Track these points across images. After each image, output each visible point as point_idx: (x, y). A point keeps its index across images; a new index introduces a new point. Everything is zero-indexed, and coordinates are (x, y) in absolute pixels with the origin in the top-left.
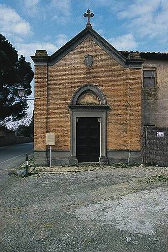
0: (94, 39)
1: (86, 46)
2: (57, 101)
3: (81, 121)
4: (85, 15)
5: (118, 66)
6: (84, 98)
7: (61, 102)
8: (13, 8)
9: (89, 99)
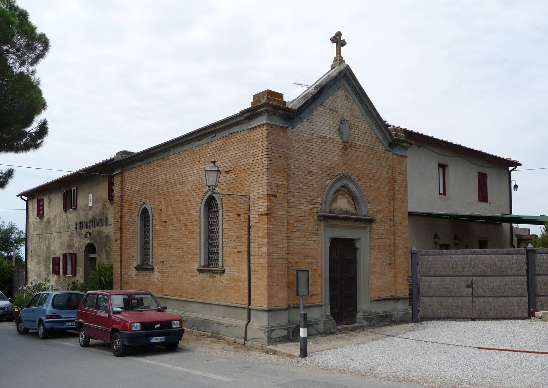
0: (349, 90)
2: (300, 204)
7: (306, 207)
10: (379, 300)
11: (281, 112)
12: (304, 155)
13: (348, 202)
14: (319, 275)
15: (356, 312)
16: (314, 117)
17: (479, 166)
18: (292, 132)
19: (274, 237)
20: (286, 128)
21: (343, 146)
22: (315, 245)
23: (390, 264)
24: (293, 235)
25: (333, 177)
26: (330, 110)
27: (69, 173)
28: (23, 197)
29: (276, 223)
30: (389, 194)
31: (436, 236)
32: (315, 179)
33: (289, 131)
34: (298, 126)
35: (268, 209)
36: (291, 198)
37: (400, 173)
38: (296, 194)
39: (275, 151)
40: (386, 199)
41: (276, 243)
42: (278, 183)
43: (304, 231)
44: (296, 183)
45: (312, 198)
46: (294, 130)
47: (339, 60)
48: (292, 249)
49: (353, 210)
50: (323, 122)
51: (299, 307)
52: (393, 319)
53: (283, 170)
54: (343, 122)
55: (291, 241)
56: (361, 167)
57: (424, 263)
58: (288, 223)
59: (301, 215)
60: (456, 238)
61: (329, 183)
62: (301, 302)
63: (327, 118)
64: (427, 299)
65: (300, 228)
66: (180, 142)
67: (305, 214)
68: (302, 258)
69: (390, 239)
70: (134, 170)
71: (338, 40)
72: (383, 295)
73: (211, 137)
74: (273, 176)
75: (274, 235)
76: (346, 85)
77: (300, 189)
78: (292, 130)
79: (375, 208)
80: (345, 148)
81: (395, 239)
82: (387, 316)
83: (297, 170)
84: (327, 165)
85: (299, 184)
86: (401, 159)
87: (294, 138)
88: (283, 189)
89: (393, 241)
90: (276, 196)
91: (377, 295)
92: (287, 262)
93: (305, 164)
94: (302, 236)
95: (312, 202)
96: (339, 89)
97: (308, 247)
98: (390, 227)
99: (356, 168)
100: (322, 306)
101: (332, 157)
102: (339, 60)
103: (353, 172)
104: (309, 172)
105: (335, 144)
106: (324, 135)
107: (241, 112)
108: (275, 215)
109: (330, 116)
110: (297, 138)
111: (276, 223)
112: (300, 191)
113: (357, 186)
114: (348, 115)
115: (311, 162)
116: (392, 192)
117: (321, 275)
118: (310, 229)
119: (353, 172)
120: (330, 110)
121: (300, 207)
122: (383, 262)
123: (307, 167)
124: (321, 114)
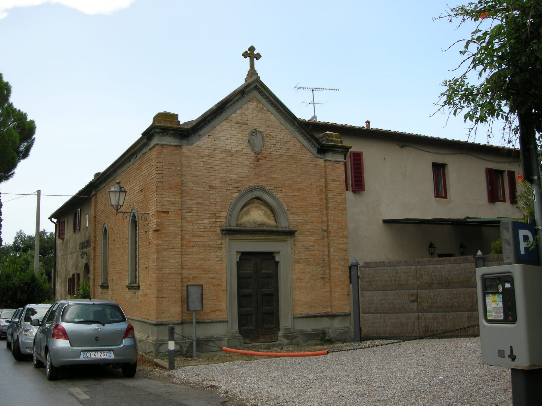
0: (264, 101)
1: (251, 111)
2: (199, 219)
3: (245, 256)
4: (245, 55)
5: (305, 151)
6: (247, 213)
7: (207, 222)
8: (515, 194)
9: (257, 216)
10: (308, 317)
11: (172, 132)
12: (204, 171)
13: (265, 214)
14: (223, 291)
15: (278, 329)
16: (216, 132)
17: (493, 161)
18: (190, 150)
19: (165, 253)
20: (180, 146)
21: (254, 158)
22: (219, 259)
23: (323, 278)
24: (191, 250)
25: (242, 190)
26: (238, 123)
27: (70, 197)
28: (53, 219)
29: (167, 239)
30: (321, 203)
31: (431, 245)
32: (218, 193)
33: (185, 150)
34: (197, 143)
35: (158, 225)
36: (188, 214)
37: (334, 180)
38: (194, 209)
39: (167, 170)
40: (316, 209)
41: (167, 259)
42: (170, 199)
43: (203, 246)
44: (194, 199)
45: (214, 212)
46: (192, 147)
47: (252, 72)
48: (189, 264)
49: (273, 223)
50: (229, 136)
51: (192, 323)
52: (327, 338)
53: (176, 187)
54: (254, 134)
55: (187, 256)
56: (280, 177)
57: (365, 276)
58: (182, 239)
59: (200, 230)
60: (462, 246)
61: (236, 195)
62: (194, 317)
63: (234, 132)
64: (368, 316)
65: (199, 243)
66: (118, 164)
67: (205, 228)
68: (201, 272)
69: (323, 251)
70: (102, 190)
71: (251, 55)
72: (314, 312)
73: (134, 158)
74: (164, 193)
75: (164, 250)
76: (259, 97)
77: (199, 204)
78: (189, 147)
79: (300, 219)
80: (257, 160)
81: (329, 251)
82: (316, 334)
83: (194, 186)
84: (233, 178)
85: (198, 199)
86: (336, 165)
87: (191, 154)
88: (176, 205)
89: (327, 253)
90: (168, 212)
91: (301, 311)
92: (180, 277)
93: (205, 179)
94: (202, 251)
95: (214, 216)
96: (250, 101)
97: (209, 262)
98: (323, 238)
99: (273, 178)
100: (227, 322)
101: (242, 170)
102: (252, 72)
103: (268, 183)
104: (211, 187)
105: (245, 157)
106: (230, 149)
107: (144, 134)
108: (166, 231)
109: (237, 130)
110: (196, 155)
111: (167, 239)
112: (199, 206)
113: (274, 197)
114: (261, 126)
115: (213, 177)
116: (325, 201)
117: (226, 291)
118: (212, 243)
119: (268, 183)
120: (238, 123)
121: (199, 222)
122: (313, 276)
123: (208, 182)
124: (226, 128)
